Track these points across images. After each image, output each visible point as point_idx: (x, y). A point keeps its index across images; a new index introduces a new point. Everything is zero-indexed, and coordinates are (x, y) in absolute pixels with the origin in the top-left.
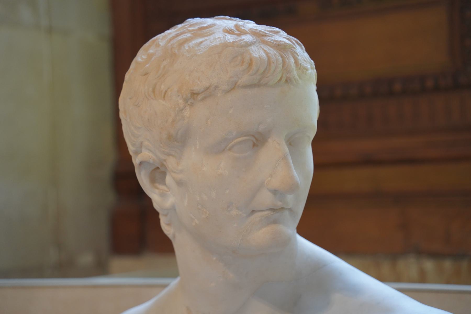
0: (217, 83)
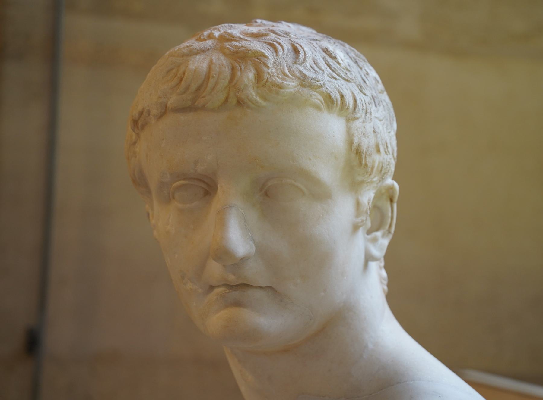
0: (148, 106)
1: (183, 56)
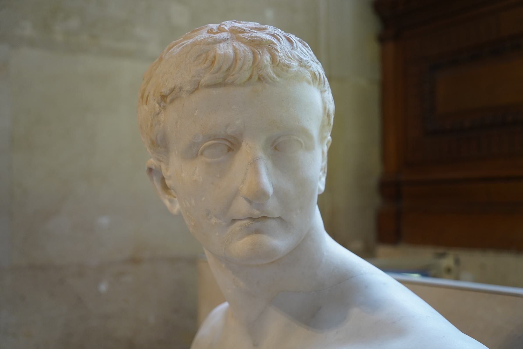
1: (208, 45)
